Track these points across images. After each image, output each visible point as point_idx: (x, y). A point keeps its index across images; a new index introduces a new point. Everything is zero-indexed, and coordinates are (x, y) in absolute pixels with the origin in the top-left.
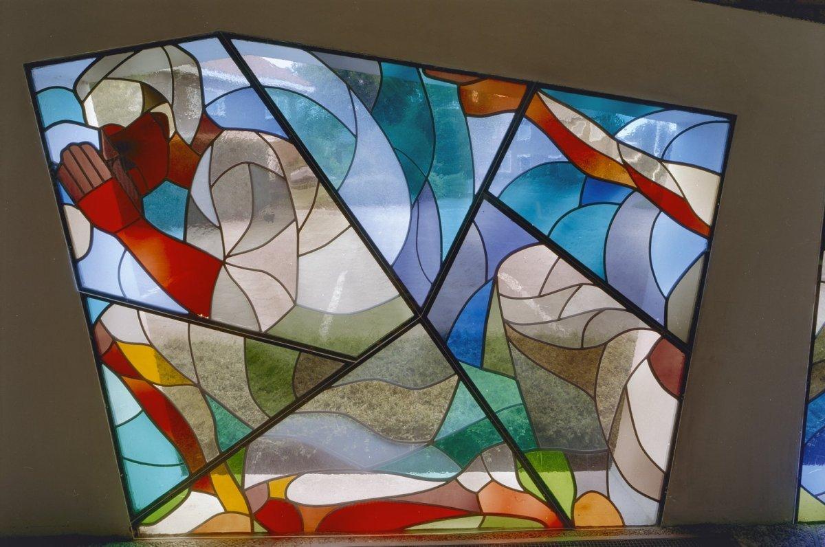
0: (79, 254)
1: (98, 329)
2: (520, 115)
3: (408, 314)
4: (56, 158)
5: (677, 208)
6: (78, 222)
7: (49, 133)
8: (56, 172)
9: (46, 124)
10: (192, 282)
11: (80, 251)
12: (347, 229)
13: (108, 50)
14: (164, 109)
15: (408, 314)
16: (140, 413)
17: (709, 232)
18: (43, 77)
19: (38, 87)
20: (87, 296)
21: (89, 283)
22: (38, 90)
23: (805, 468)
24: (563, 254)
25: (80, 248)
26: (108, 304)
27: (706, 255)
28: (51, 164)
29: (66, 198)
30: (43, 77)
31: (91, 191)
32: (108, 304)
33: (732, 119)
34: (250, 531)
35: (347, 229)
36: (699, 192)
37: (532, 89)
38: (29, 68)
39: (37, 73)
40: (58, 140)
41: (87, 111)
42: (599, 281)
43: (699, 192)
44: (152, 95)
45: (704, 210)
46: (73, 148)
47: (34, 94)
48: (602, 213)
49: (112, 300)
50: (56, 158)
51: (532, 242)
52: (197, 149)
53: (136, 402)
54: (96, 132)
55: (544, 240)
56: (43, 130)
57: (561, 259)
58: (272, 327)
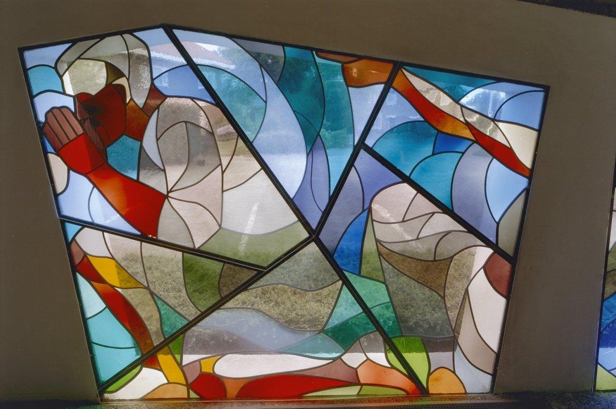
0: (59, 190)
1: (73, 246)
2: (388, 86)
3: (305, 235)
4: (42, 118)
5: (506, 155)
6: (58, 166)
7: (36, 100)
8: (42, 129)
9: (35, 93)
10: (144, 211)
11: (60, 188)
12: (259, 171)
13: (80, 37)
14: (122, 81)
15: (305, 235)
16: (105, 309)
17: (529, 174)
18: (32, 57)
19: (29, 65)
20: (65, 221)
21: (66, 212)
22: (28, 67)
23: (601, 350)
24: (420, 190)
25: (60, 186)
26: (80, 227)
27: (527, 190)
28: (38, 122)
29: (50, 148)
30: (32, 57)
31: (68, 143)
32: (80, 227)
33: (546, 89)
34: (186, 397)
35: (259, 171)
36: (522, 143)
37: (397, 67)
38: (21, 51)
39: (28, 55)
40: (44, 105)
41: (65, 83)
42: (447, 210)
43: (522, 143)
44: (113, 71)
45: (525, 157)
46: (54, 111)
47: (26, 70)
48: (449, 159)
49: (84, 224)
50: (42, 118)
51: (397, 181)
52: (147, 111)
53: (101, 301)
54: (72, 99)
55: (406, 179)
56: (32, 97)
57: (419, 194)
58: (203, 245)
